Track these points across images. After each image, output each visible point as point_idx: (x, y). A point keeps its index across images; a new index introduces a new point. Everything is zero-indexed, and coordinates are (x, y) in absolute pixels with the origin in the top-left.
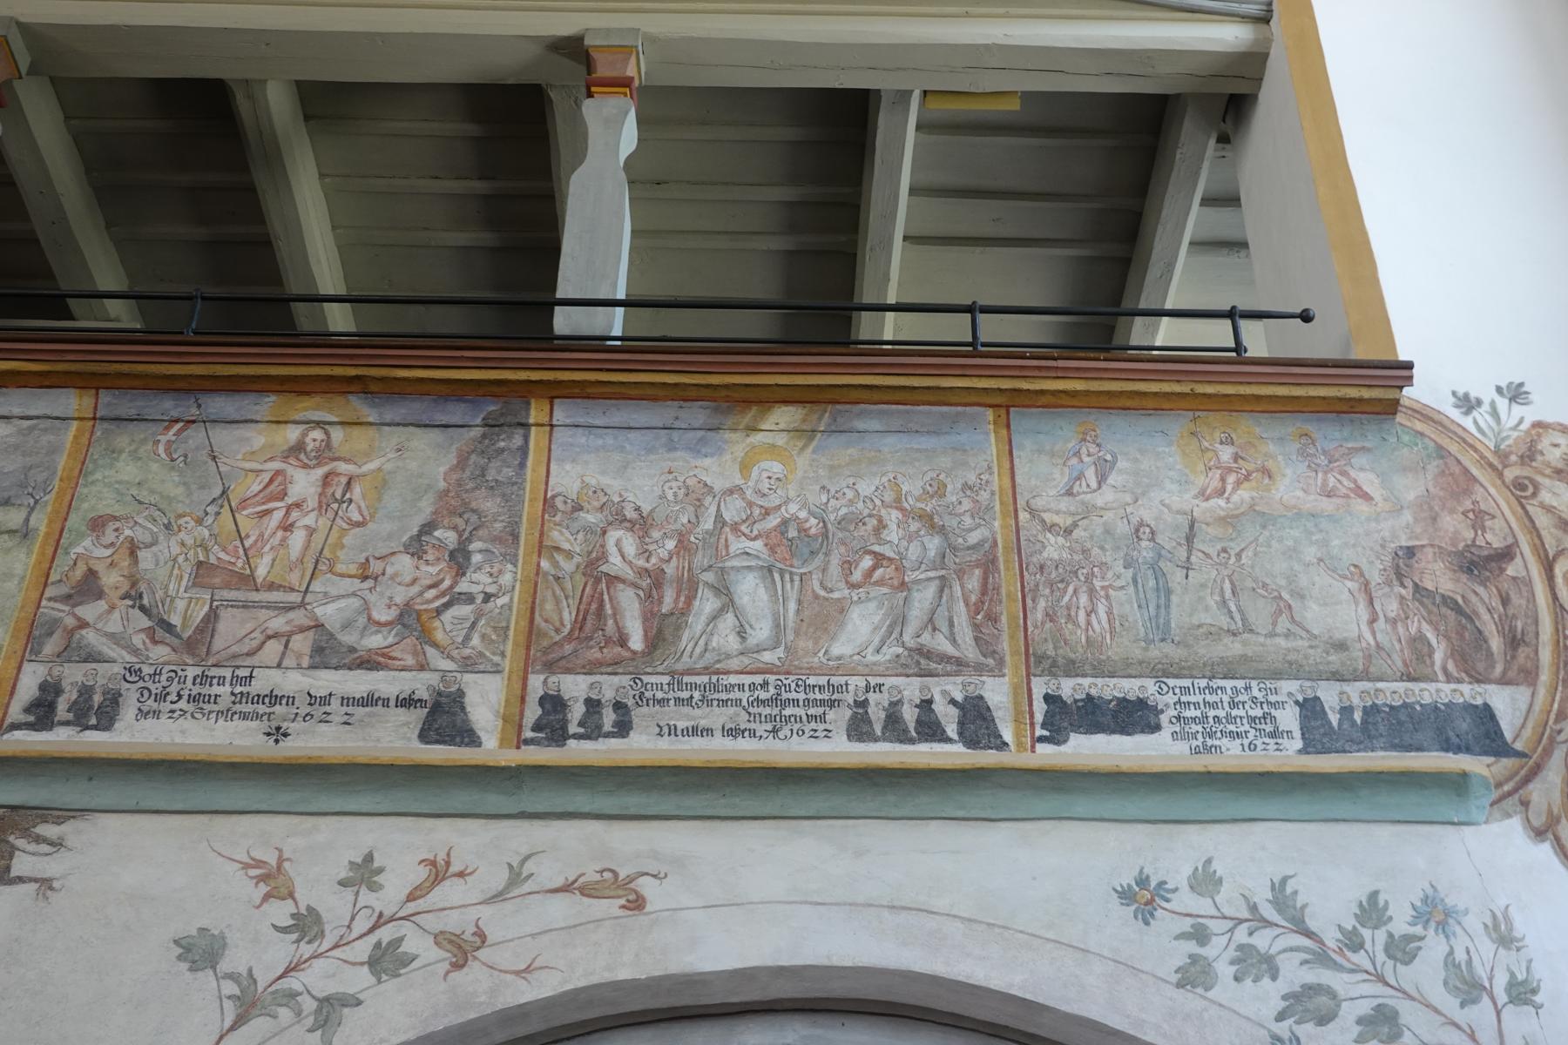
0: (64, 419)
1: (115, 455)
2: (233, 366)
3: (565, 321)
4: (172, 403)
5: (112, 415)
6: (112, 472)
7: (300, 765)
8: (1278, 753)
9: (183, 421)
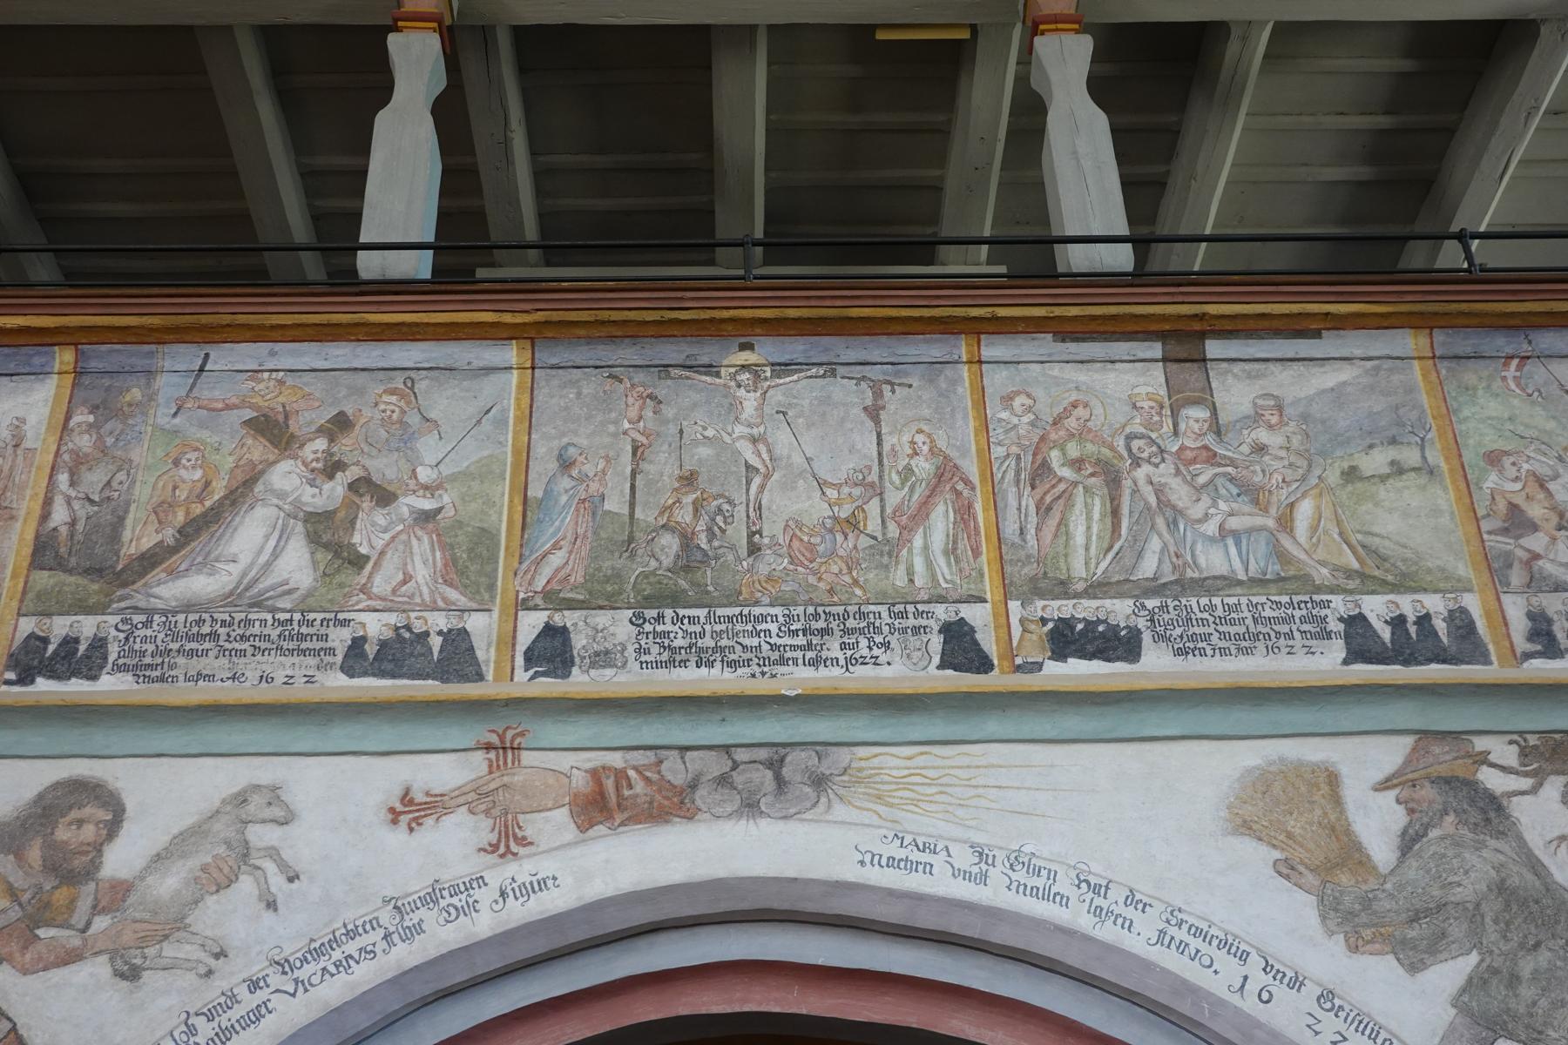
0: (1402, 359)
1: (1470, 392)
3: (369, 265)
4: (1503, 340)
5: (1450, 353)
6: (1477, 409)
7: (227, 706)
8: (309, 685)
9: (1518, 357)
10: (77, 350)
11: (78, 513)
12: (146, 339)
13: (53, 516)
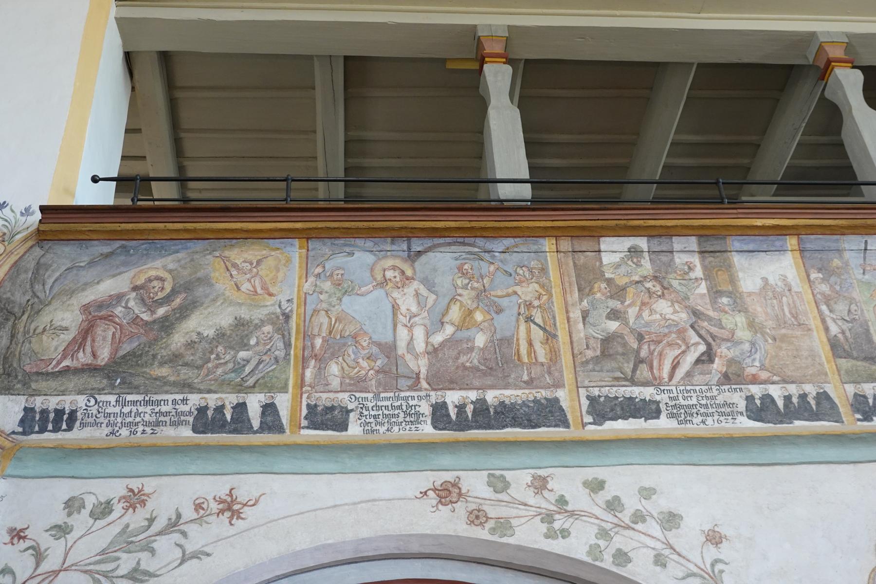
2: (332, 223)
10: (798, 238)
11: (843, 327)
12: (836, 232)
13: (830, 328)
